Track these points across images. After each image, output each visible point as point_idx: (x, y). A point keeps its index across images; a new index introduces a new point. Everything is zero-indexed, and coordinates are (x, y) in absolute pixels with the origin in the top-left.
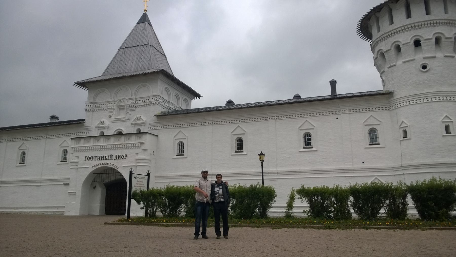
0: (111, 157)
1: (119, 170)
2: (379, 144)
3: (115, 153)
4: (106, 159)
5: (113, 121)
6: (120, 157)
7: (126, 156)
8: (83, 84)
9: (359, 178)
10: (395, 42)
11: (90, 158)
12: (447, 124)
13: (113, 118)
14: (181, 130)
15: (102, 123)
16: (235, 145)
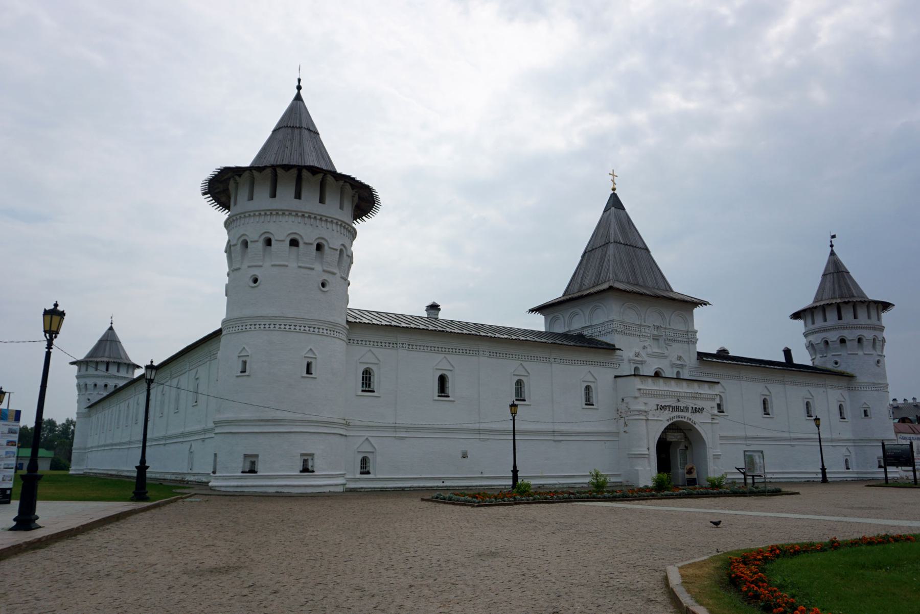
0: (686, 409)
1: (696, 426)
2: (373, 391)
3: (691, 404)
4: (682, 411)
5: (649, 355)
6: (697, 410)
7: (703, 409)
8: (796, 316)
9: (333, 436)
10: (323, 238)
11: (663, 408)
12: (310, 360)
13: (649, 350)
14: (372, 349)
15: (680, 358)
16: (375, 380)
